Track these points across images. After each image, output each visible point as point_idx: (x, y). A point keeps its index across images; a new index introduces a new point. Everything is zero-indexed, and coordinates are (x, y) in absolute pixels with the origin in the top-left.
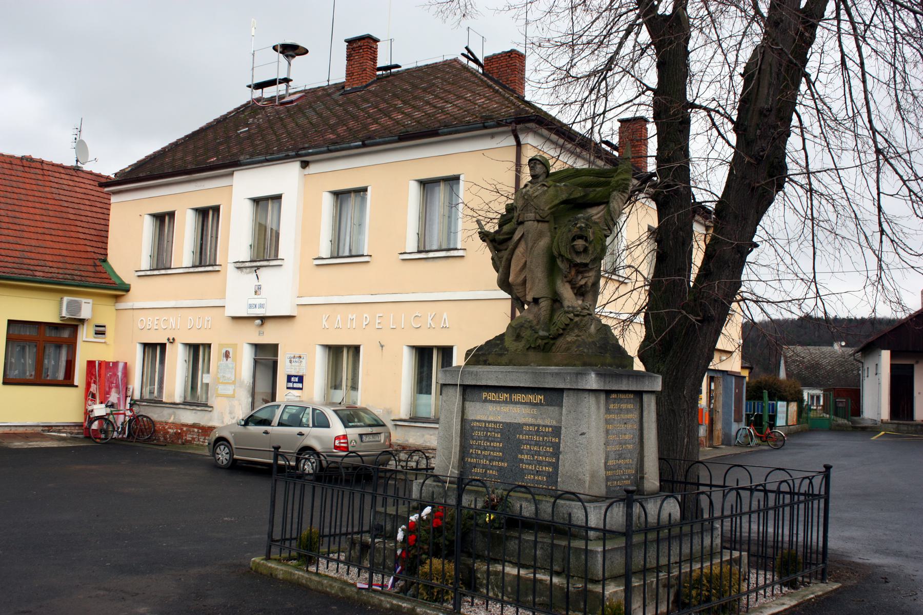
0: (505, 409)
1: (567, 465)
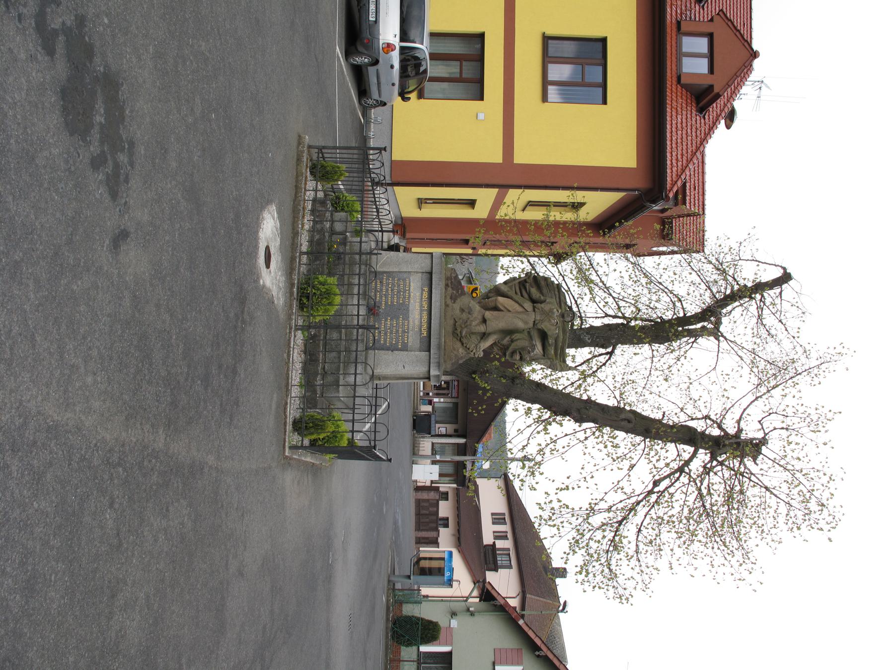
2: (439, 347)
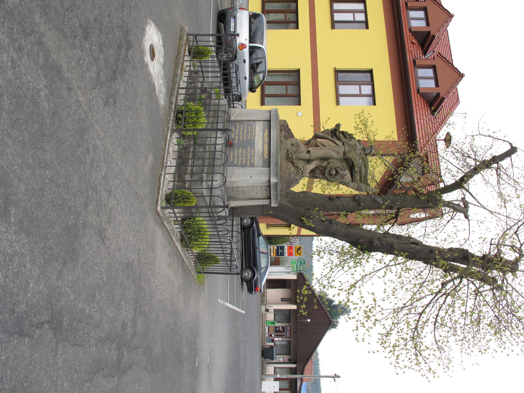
0: (261, 141)
2: (277, 164)
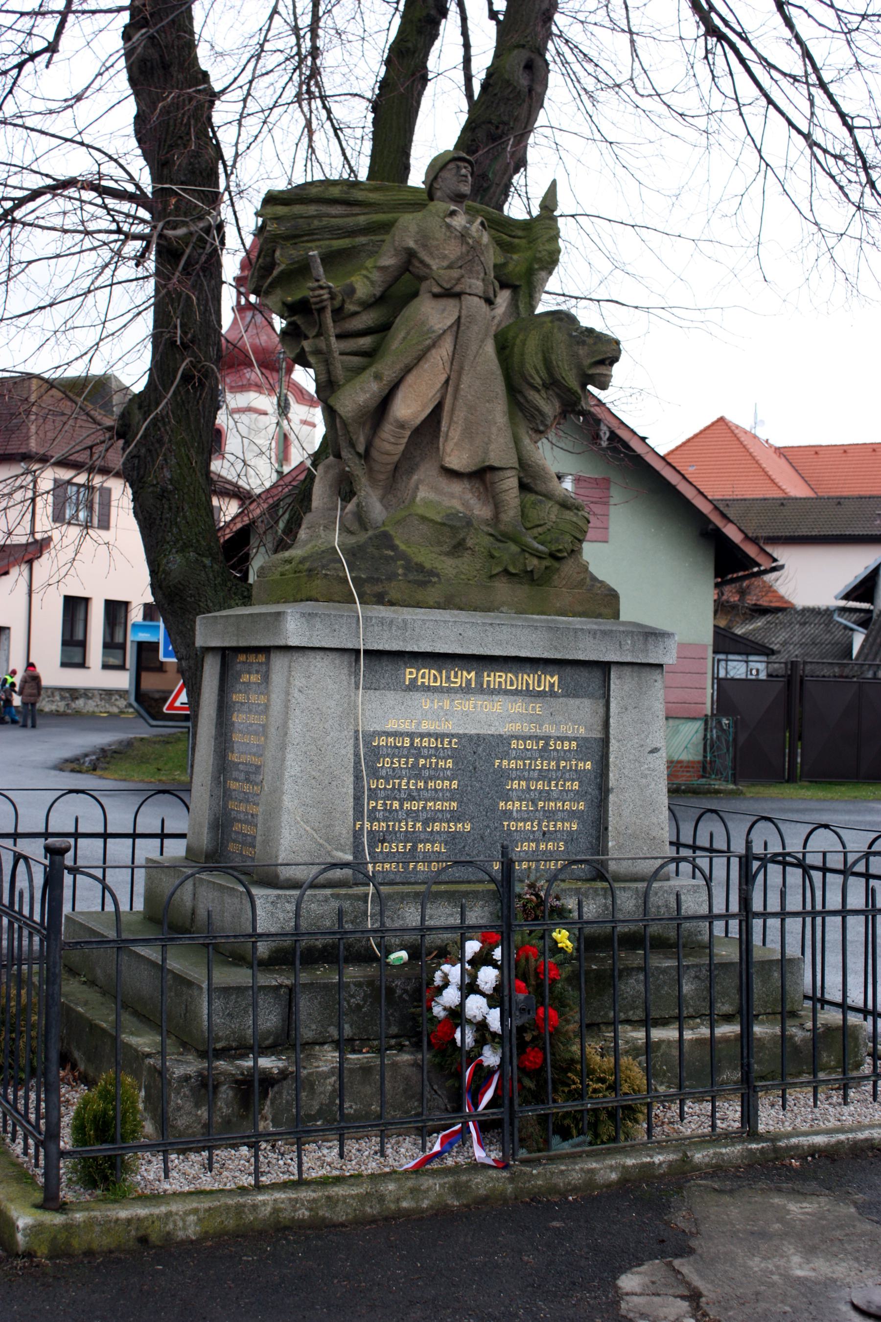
1: (626, 813)
